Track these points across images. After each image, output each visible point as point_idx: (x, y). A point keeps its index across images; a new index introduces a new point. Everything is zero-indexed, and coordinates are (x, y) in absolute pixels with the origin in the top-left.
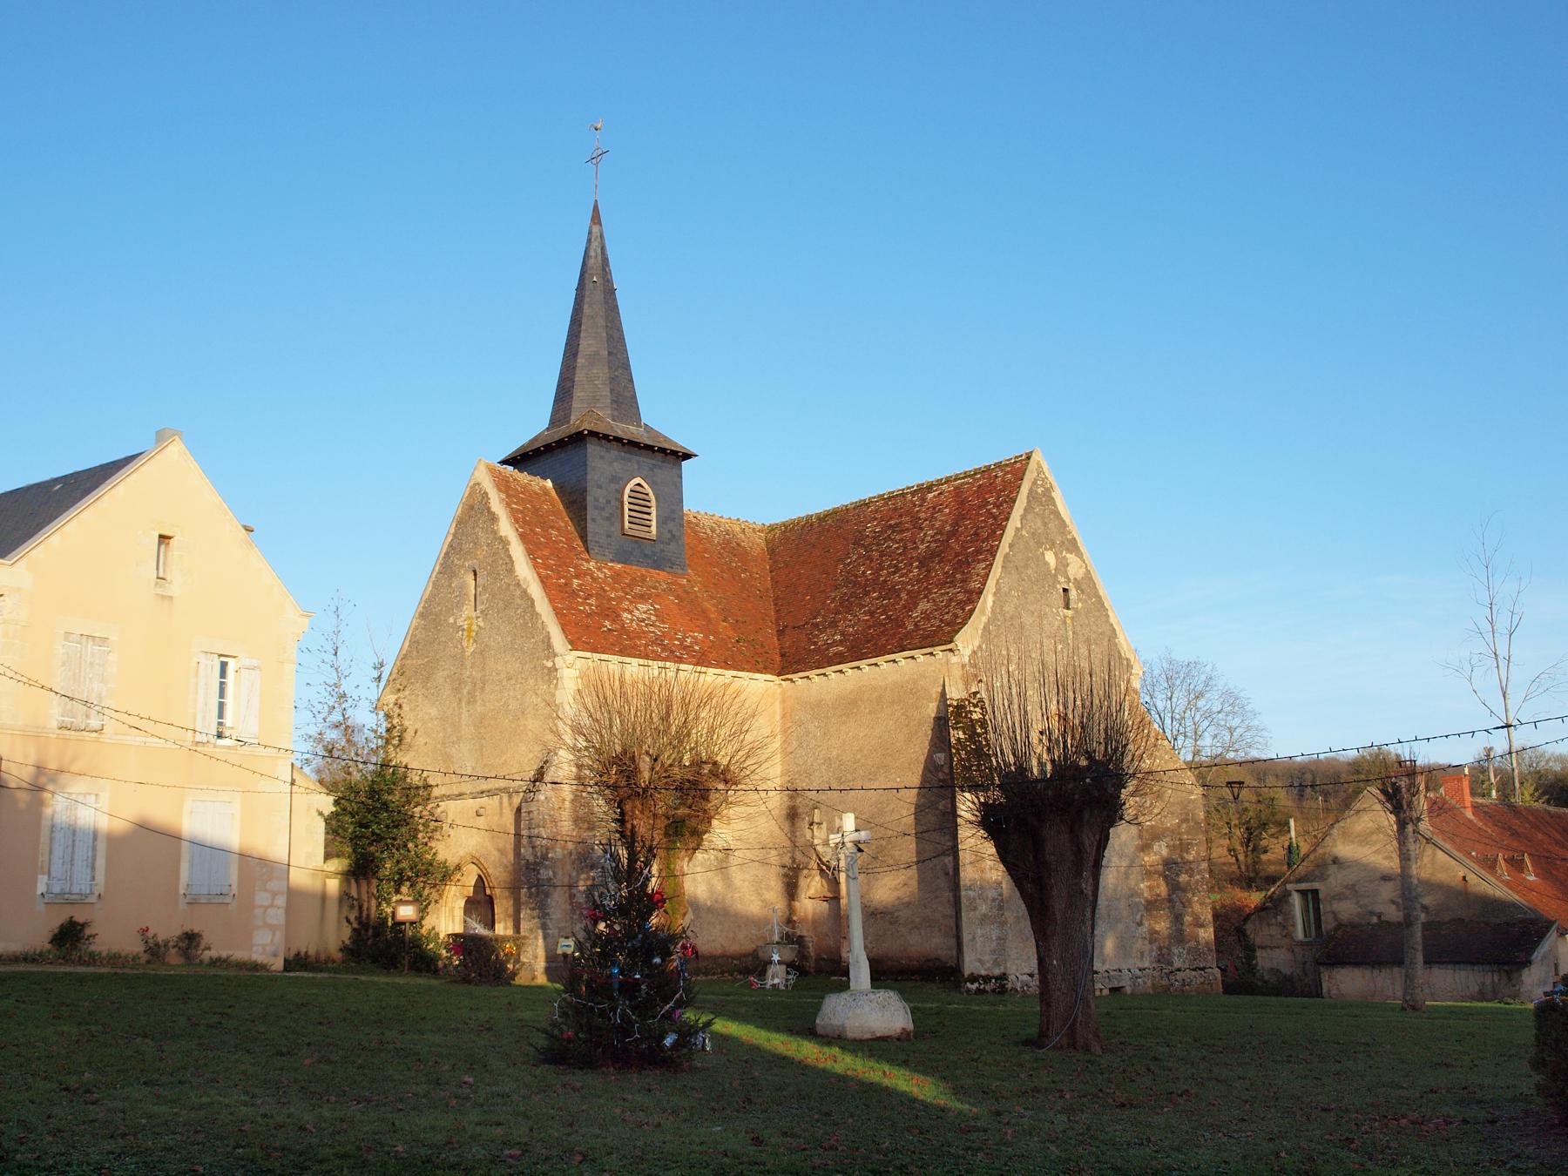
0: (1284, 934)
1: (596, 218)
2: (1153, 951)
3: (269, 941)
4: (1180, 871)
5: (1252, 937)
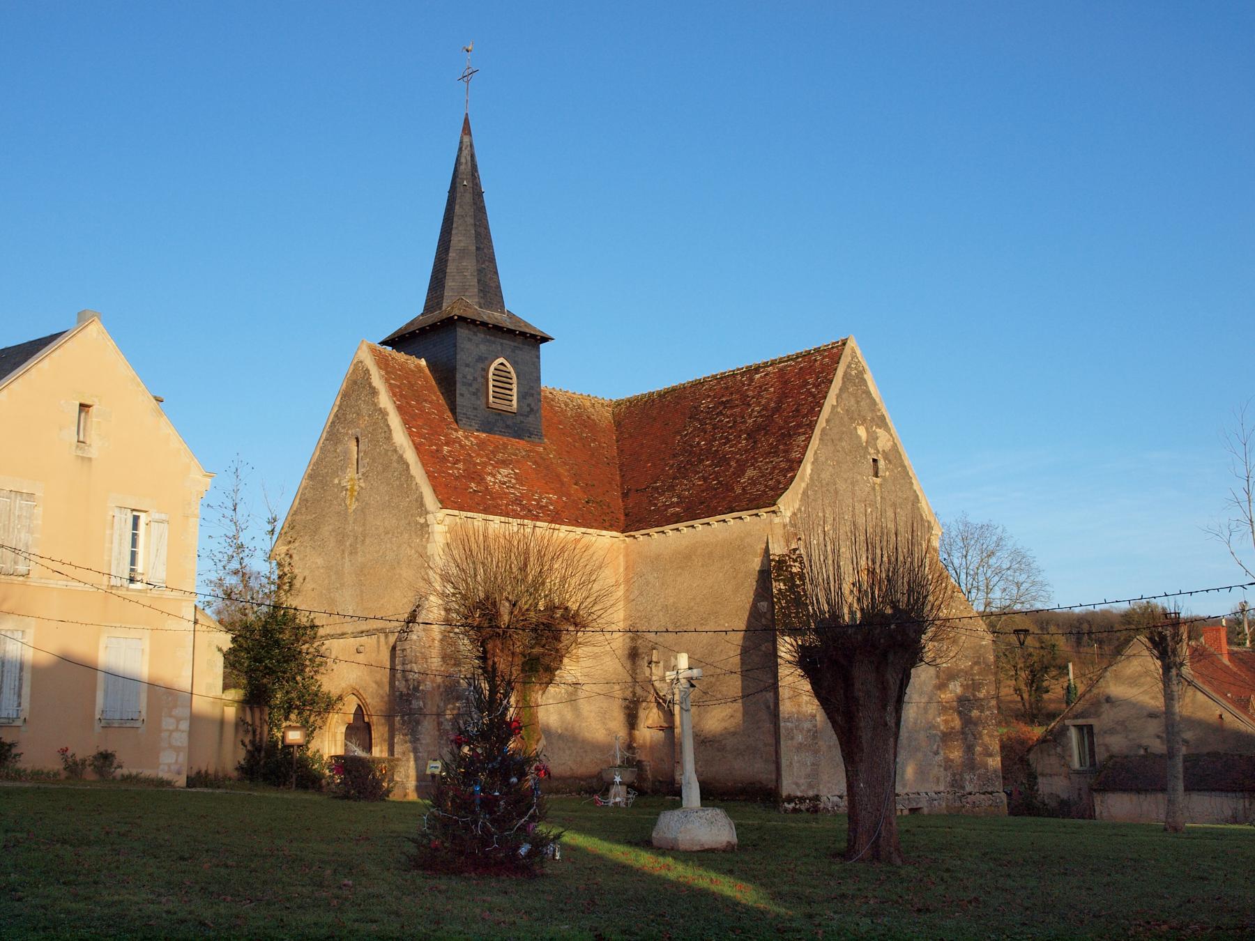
1: (467, 129)
3: (173, 761)
5: (1034, 766)
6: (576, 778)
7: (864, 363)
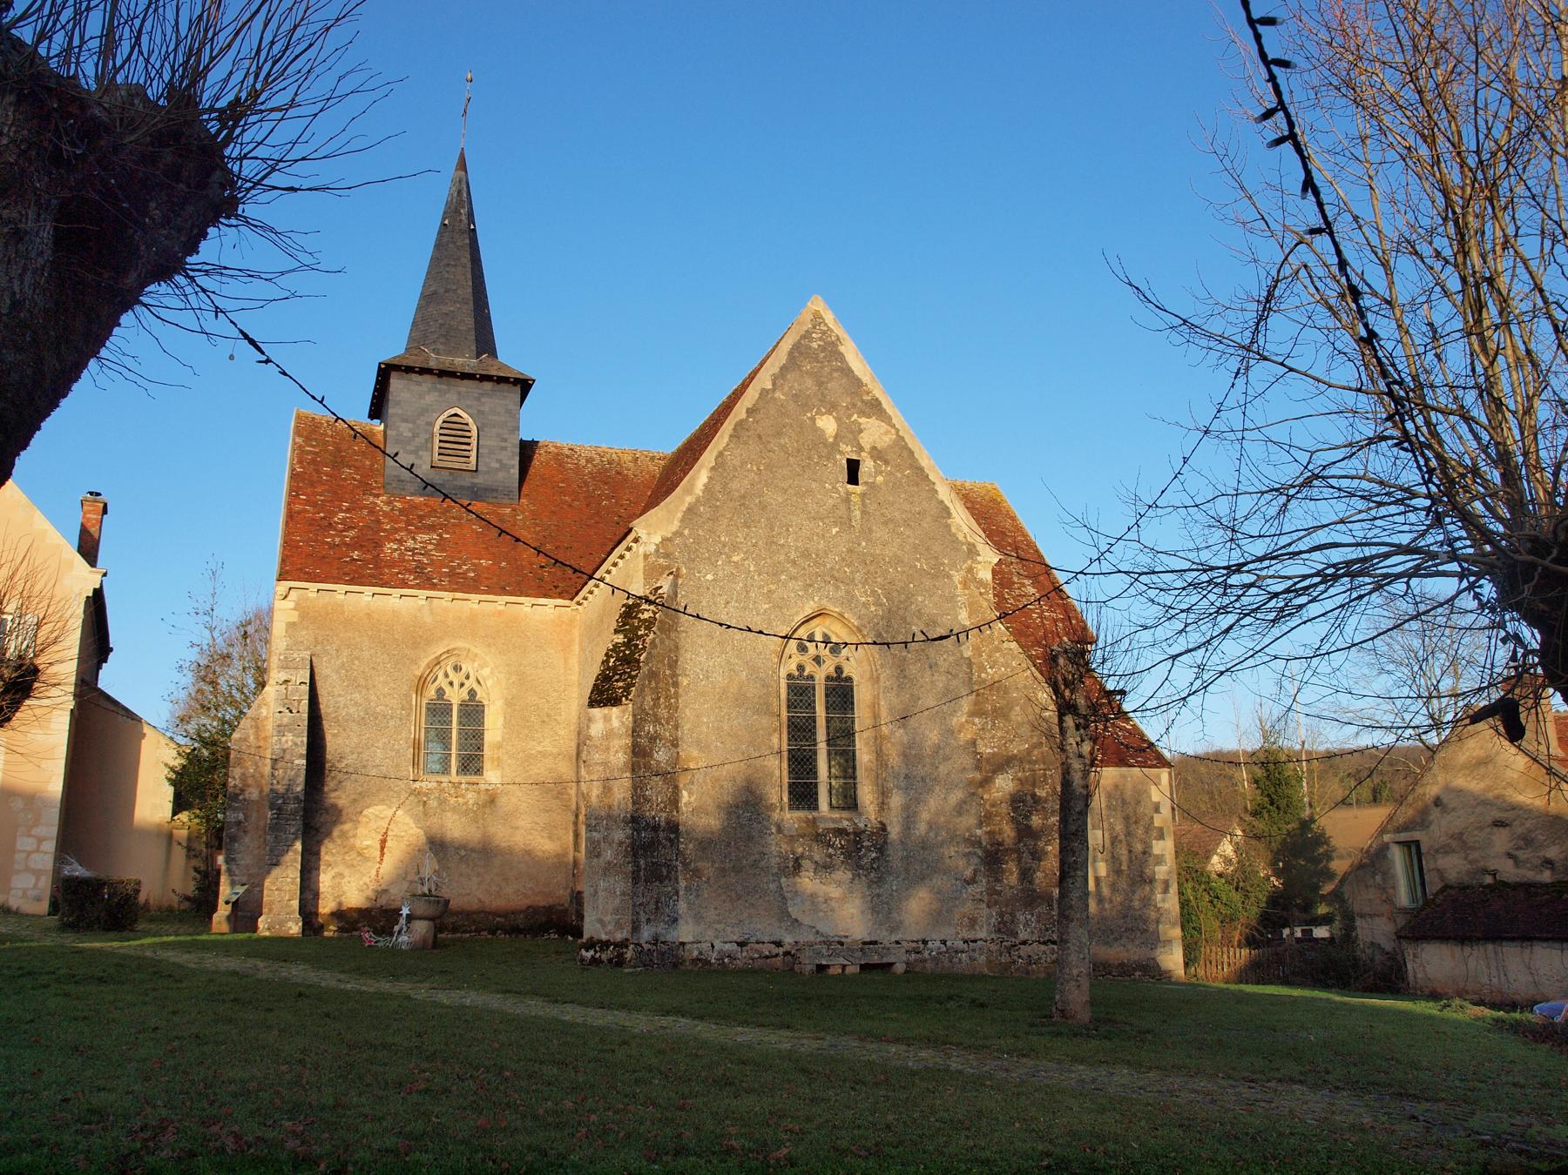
0: (1384, 898)
1: (462, 165)
3: (31, 886)
4: (1029, 811)
6: (489, 913)
7: (839, 331)
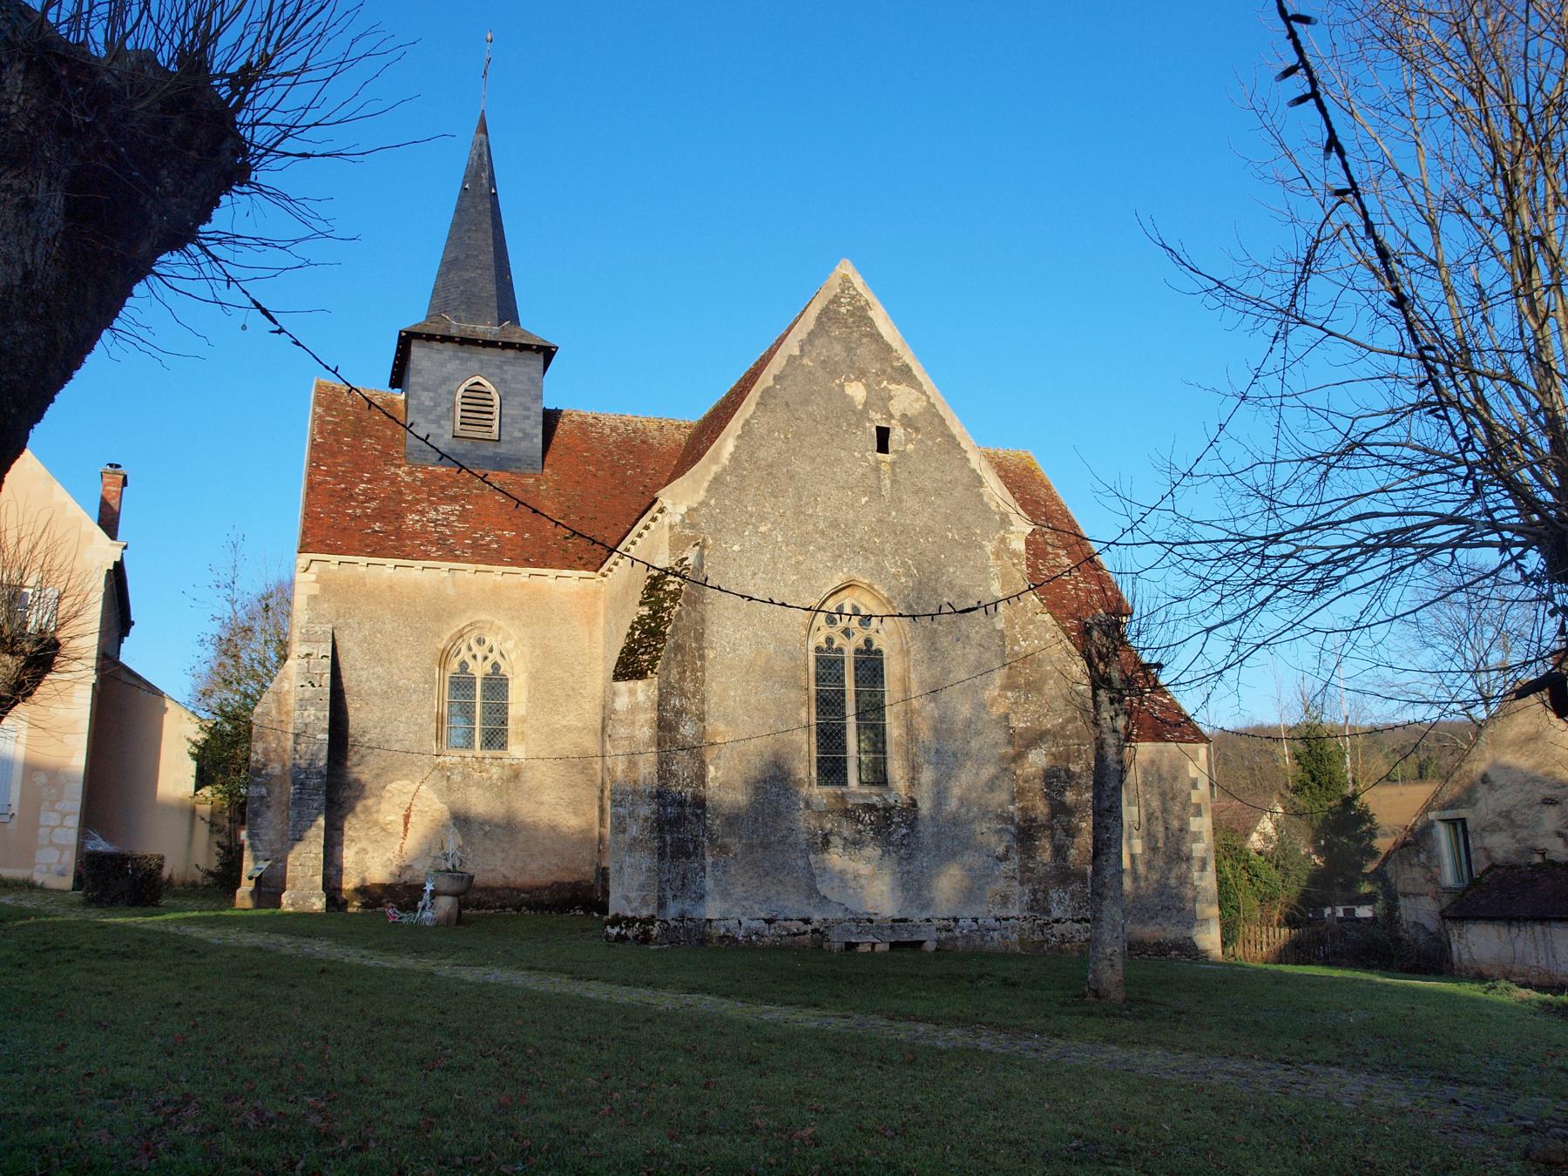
1: (483, 128)
2: (1025, 894)
3: (55, 861)
5: (1393, 881)
6: (514, 889)
